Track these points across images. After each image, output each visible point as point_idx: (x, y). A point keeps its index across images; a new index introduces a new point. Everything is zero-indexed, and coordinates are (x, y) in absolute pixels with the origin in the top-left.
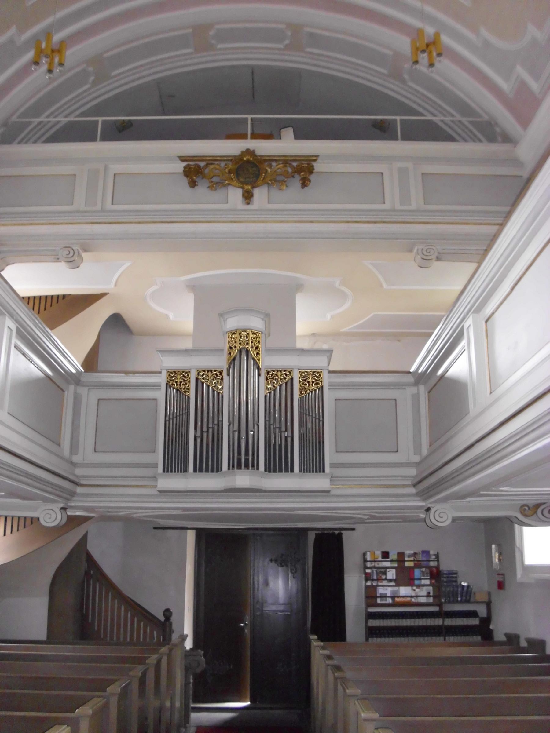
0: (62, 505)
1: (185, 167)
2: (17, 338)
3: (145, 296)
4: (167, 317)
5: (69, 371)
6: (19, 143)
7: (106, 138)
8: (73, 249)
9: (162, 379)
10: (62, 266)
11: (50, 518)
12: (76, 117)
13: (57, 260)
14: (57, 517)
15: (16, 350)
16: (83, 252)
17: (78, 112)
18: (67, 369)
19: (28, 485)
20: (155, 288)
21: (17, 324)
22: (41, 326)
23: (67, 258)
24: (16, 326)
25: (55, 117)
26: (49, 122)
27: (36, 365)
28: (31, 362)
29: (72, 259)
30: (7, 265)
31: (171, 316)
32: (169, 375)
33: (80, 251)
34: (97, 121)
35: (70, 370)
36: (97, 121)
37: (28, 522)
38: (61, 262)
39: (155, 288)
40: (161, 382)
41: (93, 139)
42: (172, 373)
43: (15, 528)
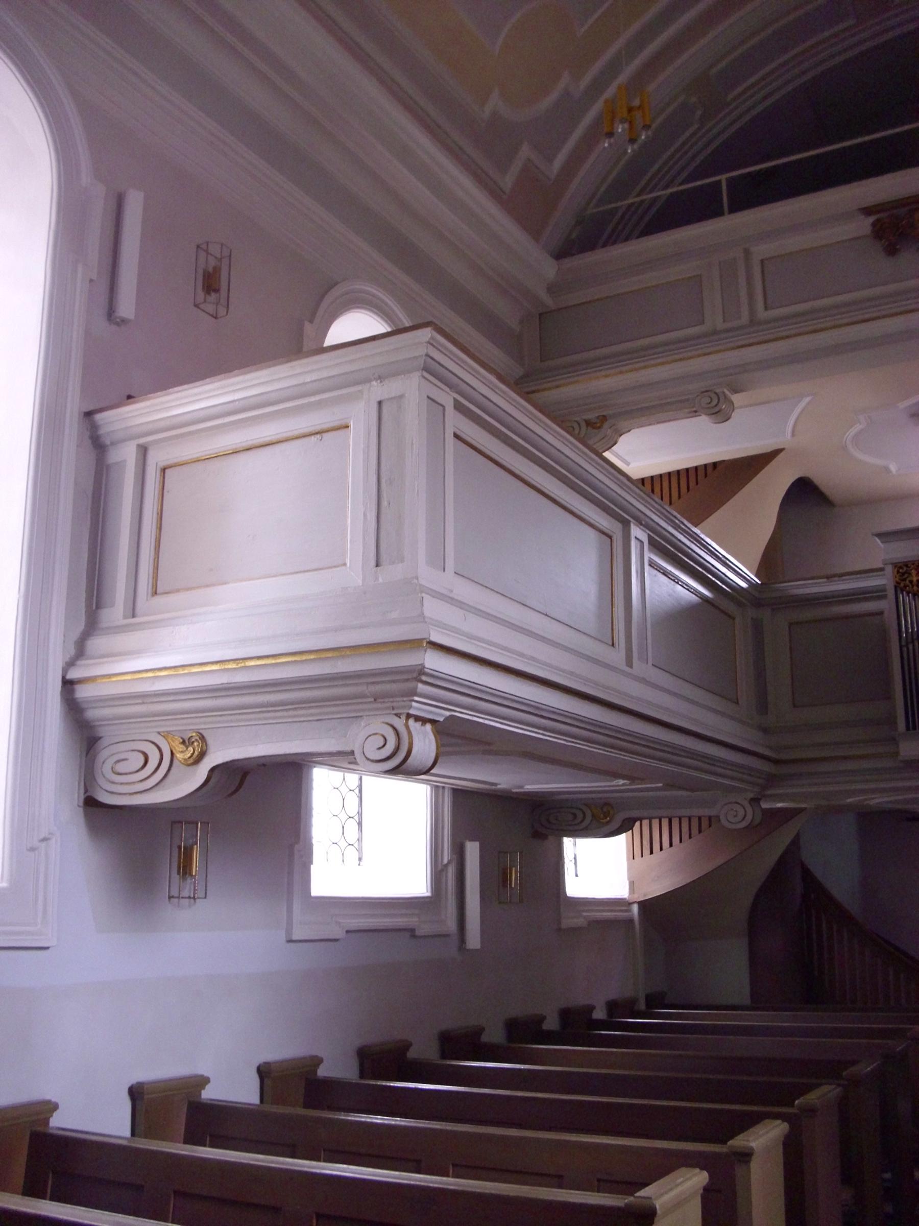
0: (751, 795)
1: (874, 225)
2: (650, 550)
3: (844, 440)
4: (887, 469)
5: (738, 587)
6: (604, 246)
7: (737, 206)
8: (716, 393)
9: (886, 580)
10: (703, 421)
11: (735, 816)
12: (681, 184)
13: (695, 413)
14: (746, 811)
15: (652, 569)
16: (732, 394)
17: (684, 175)
18: (734, 584)
19: (696, 769)
20: (858, 428)
21: (648, 532)
22: (683, 527)
23: (709, 408)
24: (647, 536)
25: (651, 192)
26: (642, 202)
27: (685, 586)
28: (678, 583)
29: (716, 410)
30: (621, 435)
31: (893, 468)
32: (898, 572)
33: (727, 392)
34: (720, 182)
35: (739, 585)
36: (720, 182)
37: (705, 823)
38: (700, 415)
39: (858, 428)
40: (884, 585)
41: (717, 213)
42: (901, 568)
43: (676, 839)
